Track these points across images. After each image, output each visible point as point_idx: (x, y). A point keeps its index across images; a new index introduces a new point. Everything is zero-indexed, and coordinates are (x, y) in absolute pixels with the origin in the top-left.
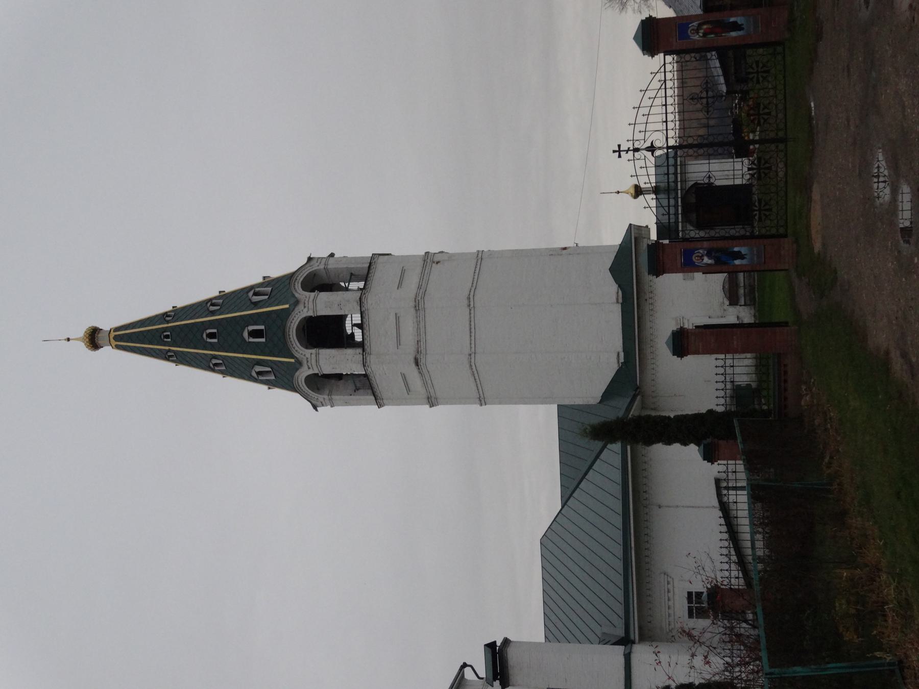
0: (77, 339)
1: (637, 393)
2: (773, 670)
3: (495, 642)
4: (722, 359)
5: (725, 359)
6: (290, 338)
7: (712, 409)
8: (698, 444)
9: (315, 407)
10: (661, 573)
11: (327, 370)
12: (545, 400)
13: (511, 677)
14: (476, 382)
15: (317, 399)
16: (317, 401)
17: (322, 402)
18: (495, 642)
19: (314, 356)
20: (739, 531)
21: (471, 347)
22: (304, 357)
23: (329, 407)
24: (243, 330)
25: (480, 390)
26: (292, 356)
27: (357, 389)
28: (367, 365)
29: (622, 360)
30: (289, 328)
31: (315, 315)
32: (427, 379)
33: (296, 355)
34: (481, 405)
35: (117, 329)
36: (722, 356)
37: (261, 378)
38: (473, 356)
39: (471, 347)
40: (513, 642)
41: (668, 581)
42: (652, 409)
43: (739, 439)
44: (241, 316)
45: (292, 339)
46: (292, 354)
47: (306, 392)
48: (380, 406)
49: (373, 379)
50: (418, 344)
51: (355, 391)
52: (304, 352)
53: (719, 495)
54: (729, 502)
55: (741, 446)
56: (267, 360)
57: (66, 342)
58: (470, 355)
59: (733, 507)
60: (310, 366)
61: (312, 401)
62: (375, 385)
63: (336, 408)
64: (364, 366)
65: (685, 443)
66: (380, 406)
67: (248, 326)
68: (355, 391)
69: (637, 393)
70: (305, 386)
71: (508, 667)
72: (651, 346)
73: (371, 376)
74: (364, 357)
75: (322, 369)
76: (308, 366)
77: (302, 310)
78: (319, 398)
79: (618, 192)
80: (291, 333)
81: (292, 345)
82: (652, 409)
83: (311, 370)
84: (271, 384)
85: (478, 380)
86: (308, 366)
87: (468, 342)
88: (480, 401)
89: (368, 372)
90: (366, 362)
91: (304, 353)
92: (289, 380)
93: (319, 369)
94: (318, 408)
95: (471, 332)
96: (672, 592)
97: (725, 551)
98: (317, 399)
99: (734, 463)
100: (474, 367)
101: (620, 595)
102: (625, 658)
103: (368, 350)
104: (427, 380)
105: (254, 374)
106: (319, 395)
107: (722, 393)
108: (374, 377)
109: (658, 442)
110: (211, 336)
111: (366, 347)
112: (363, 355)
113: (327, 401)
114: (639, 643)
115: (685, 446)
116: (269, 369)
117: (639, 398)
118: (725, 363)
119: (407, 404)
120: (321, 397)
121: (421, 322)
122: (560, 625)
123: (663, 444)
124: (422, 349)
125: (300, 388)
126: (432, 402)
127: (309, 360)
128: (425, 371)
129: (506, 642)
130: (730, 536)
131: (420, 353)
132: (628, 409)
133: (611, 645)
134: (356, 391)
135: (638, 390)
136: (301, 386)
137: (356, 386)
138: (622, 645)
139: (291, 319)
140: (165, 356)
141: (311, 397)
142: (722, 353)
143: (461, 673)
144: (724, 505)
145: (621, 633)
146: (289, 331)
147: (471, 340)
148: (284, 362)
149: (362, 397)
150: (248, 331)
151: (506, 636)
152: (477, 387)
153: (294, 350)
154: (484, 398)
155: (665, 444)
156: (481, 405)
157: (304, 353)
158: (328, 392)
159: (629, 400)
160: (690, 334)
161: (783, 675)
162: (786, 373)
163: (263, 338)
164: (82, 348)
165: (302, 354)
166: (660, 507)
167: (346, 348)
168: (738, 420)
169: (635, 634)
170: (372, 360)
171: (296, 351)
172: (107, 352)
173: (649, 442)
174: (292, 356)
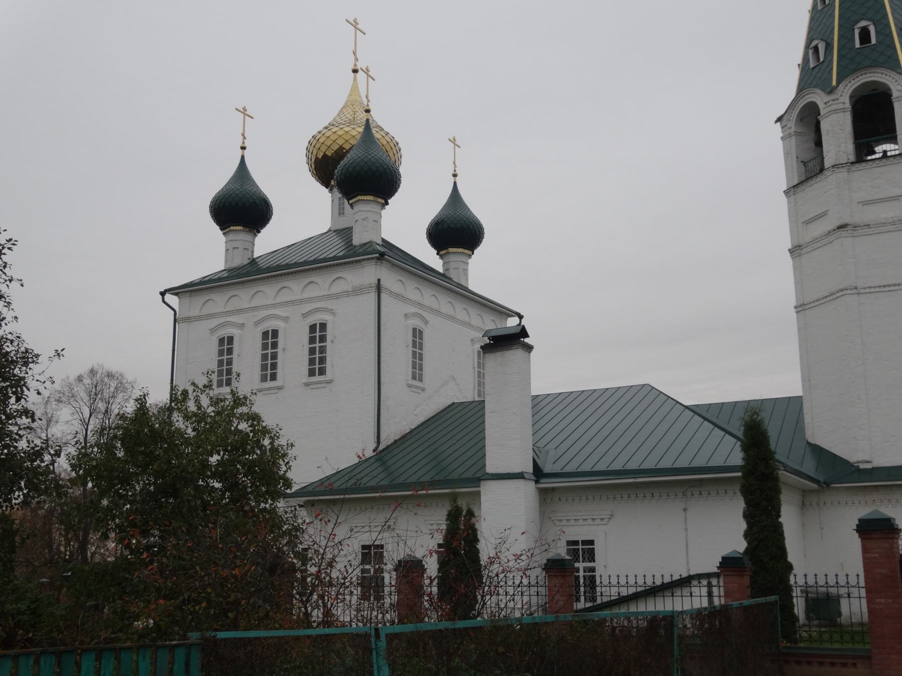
1: (822, 484)
2: (383, 638)
3: (527, 336)
4: (858, 583)
5: (859, 587)
6: (861, 75)
7: (793, 570)
8: (746, 552)
9: (779, 119)
10: (612, 512)
11: (824, 126)
12: (806, 380)
13: (492, 354)
14: (823, 298)
15: (790, 120)
16: (787, 120)
17: (786, 126)
18: (527, 336)
19: (841, 106)
20: (657, 598)
21: (865, 288)
22: (839, 94)
23: (782, 135)
24: (869, 20)
25: (813, 305)
26: (839, 82)
27: (804, 163)
28: (834, 169)
29: (862, 466)
30: (875, 72)
31: (893, 100)
32: (822, 242)
33: (840, 85)
34: (796, 307)
36: (862, 583)
37: (811, 52)
38: (855, 291)
39: (865, 288)
40: (529, 355)
41: (604, 519)
42: (803, 502)
43: (746, 602)
44: (886, 14)
45: (860, 77)
46: (842, 81)
47: (797, 106)
48: (786, 193)
49: (818, 179)
50: (866, 226)
51: (802, 162)
52: (846, 94)
53: (700, 577)
54: (691, 587)
55: (735, 604)
56: (833, 54)
58: (856, 288)
59: (686, 591)
60: (828, 104)
61: (787, 114)
62: (811, 182)
63: (780, 143)
64: (833, 166)
65: (747, 535)
66: (786, 193)
67: (874, 24)
68: (802, 162)
69: (822, 484)
70: (805, 102)
71: (502, 351)
72: (882, 500)
73: (821, 177)
74: (845, 165)
75: (826, 119)
76: (829, 102)
77: (899, 84)
78: (790, 122)
80: (868, 75)
81: (854, 79)
82: (803, 502)
83: (824, 106)
84: (804, 67)
85: (825, 300)
86: (829, 102)
87: (872, 285)
88: (801, 306)
89: (825, 172)
90: (838, 168)
91: (844, 94)
92: (811, 83)
93: (826, 115)
94: (779, 123)
95: (884, 286)
96: (600, 523)
97: (632, 581)
98: (790, 120)
99: (721, 595)
100: (841, 294)
101: (586, 467)
102: (519, 473)
103: (854, 168)
104: (821, 242)
105: (814, 43)
106: (794, 122)
107: (832, 582)
108: (820, 181)
109: (746, 503)
111: (857, 165)
112: (846, 163)
113: (788, 132)
114: (538, 488)
115: (744, 536)
116: (822, 59)
117: (815, 486)
118: (853, 587)
119: (791, 222)
120: (792, 124)
121: (894, 226)
122: (561, 407)
123: (744, 509)
124: (860, 231)
125: (802, 98)
126: (796, 251)
127: (836, 102)
128: (831, 238)
129: (529, 348)
130: (658, 586)
131: (854, 229)
132: (787, 469)
133: (534, 459)
134: (802, 163)
135: (825, 486)
136: (804, 98)
137: (808, 162)
138: (533, 471)
139: (886, 73)
141: (792, 113)
142: (866, 582)
143: (513, 314)
144: (687, 582)
145: (548, 469)
146: (870, 73)
147: (875, 287)
148: (832, 73)
149: (795, 170)
150: (869, 25)
151: (534, 347)
152: (817, 301)
153: (846, 83)
154: (804, 310)
155: (744, 511)
156: (796, 307)
157: (844, 94)
158: (799, 131)
159: (815, 477)
160: (890, 541)
161: (374, 653)
162: (845, 665)
163: (861, 44)
165: (843, 92)
166: (685, 510)
167: (854, 143)
168: (776, 602)
169: (546, 484)
170: (842, 174)
171: (847, 85)
173: (747, 493)
174: (839, 82)
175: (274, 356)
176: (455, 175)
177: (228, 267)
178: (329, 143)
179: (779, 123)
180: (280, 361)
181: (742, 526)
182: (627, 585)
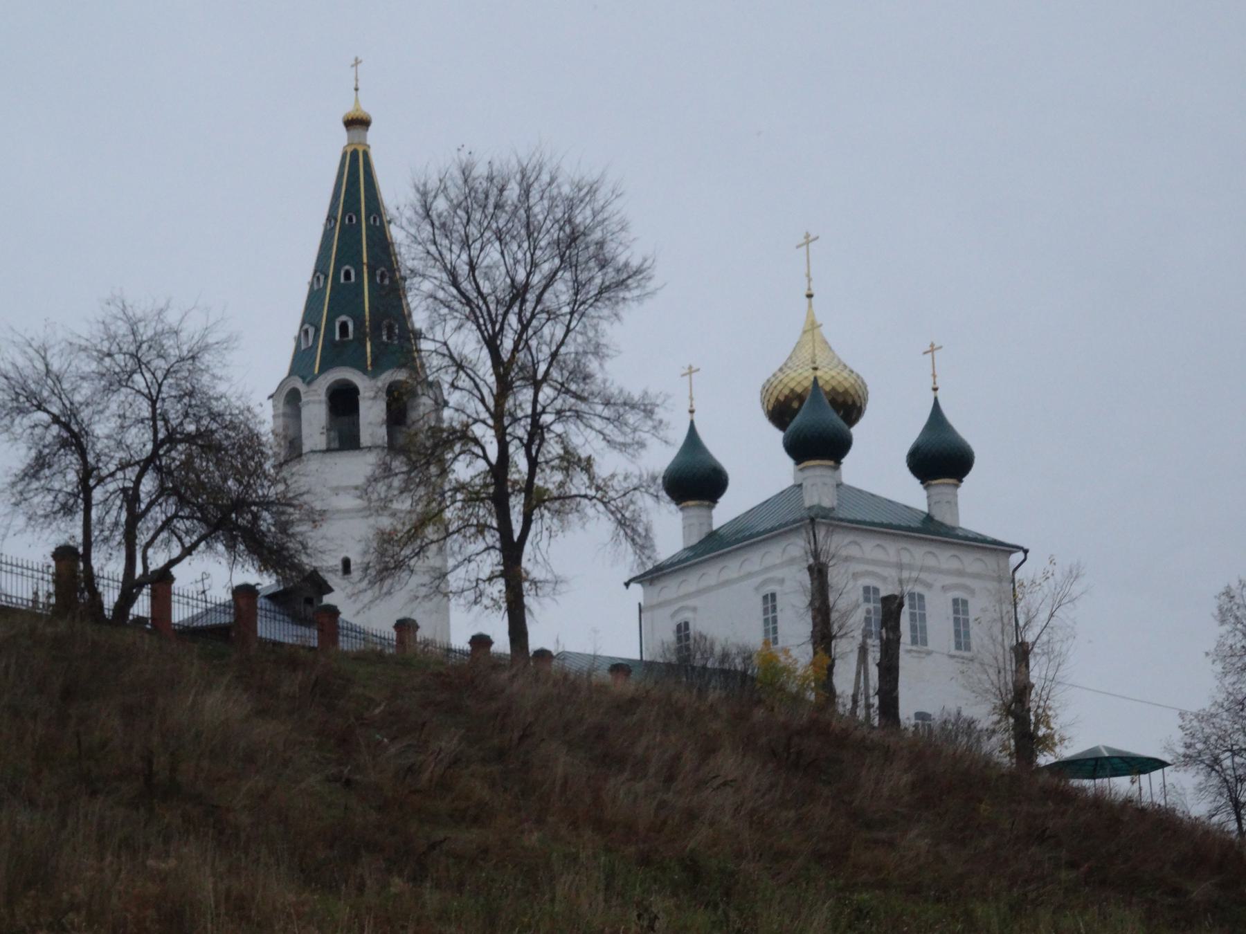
0: (357, 100)
9: (271, 397)
19: (316, 398)
24: (351, 265)
35: (366, 154)
57: (805, 292)
79: (356, 89)
110: (350, 219)
120: (281, 405)
140: (331, 217)
164: (346, 108)
172: (340, 139)
175: (775, 620)
176: (692, 412)
177: (686, 546)
178: (799, 379)
179: (271, 400)
180: (780, 623)
181: (810, 628)
182: (211, 603)
